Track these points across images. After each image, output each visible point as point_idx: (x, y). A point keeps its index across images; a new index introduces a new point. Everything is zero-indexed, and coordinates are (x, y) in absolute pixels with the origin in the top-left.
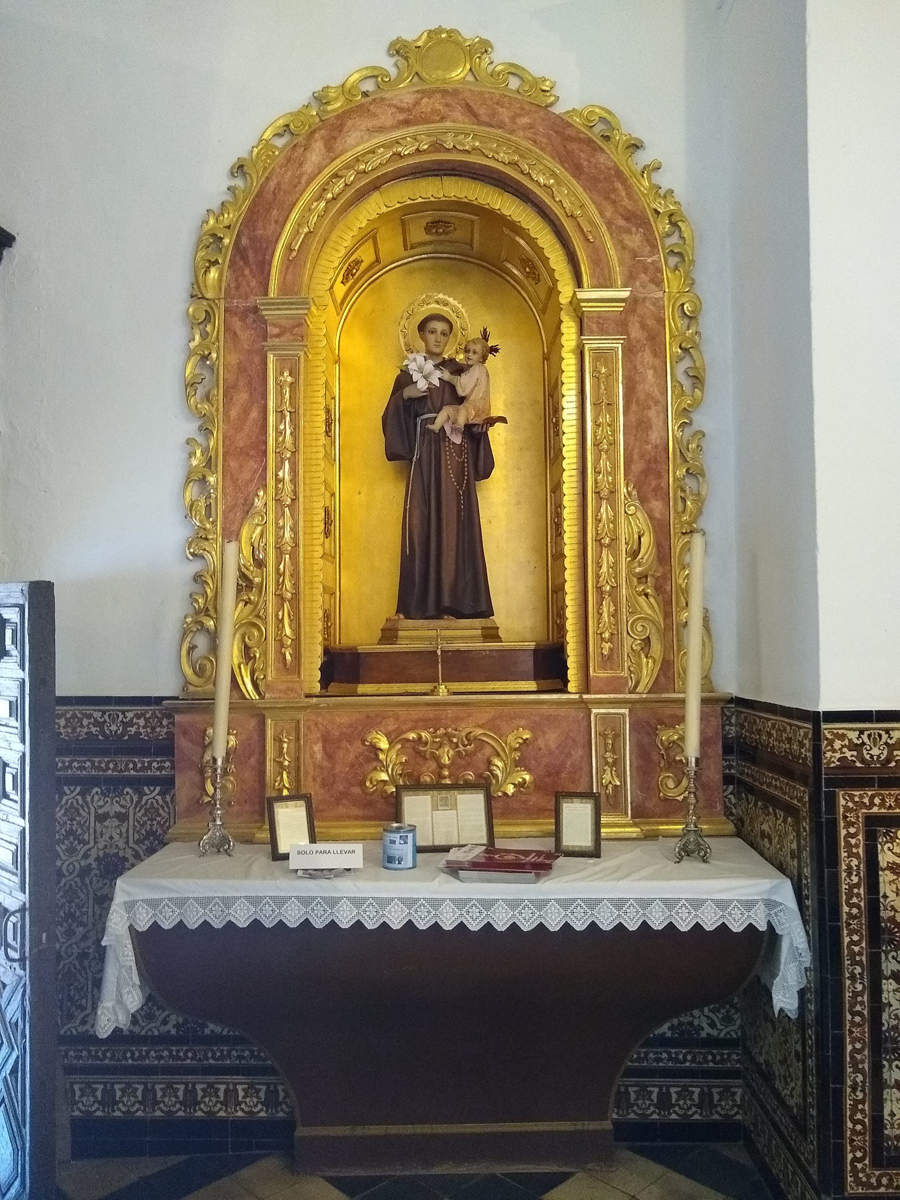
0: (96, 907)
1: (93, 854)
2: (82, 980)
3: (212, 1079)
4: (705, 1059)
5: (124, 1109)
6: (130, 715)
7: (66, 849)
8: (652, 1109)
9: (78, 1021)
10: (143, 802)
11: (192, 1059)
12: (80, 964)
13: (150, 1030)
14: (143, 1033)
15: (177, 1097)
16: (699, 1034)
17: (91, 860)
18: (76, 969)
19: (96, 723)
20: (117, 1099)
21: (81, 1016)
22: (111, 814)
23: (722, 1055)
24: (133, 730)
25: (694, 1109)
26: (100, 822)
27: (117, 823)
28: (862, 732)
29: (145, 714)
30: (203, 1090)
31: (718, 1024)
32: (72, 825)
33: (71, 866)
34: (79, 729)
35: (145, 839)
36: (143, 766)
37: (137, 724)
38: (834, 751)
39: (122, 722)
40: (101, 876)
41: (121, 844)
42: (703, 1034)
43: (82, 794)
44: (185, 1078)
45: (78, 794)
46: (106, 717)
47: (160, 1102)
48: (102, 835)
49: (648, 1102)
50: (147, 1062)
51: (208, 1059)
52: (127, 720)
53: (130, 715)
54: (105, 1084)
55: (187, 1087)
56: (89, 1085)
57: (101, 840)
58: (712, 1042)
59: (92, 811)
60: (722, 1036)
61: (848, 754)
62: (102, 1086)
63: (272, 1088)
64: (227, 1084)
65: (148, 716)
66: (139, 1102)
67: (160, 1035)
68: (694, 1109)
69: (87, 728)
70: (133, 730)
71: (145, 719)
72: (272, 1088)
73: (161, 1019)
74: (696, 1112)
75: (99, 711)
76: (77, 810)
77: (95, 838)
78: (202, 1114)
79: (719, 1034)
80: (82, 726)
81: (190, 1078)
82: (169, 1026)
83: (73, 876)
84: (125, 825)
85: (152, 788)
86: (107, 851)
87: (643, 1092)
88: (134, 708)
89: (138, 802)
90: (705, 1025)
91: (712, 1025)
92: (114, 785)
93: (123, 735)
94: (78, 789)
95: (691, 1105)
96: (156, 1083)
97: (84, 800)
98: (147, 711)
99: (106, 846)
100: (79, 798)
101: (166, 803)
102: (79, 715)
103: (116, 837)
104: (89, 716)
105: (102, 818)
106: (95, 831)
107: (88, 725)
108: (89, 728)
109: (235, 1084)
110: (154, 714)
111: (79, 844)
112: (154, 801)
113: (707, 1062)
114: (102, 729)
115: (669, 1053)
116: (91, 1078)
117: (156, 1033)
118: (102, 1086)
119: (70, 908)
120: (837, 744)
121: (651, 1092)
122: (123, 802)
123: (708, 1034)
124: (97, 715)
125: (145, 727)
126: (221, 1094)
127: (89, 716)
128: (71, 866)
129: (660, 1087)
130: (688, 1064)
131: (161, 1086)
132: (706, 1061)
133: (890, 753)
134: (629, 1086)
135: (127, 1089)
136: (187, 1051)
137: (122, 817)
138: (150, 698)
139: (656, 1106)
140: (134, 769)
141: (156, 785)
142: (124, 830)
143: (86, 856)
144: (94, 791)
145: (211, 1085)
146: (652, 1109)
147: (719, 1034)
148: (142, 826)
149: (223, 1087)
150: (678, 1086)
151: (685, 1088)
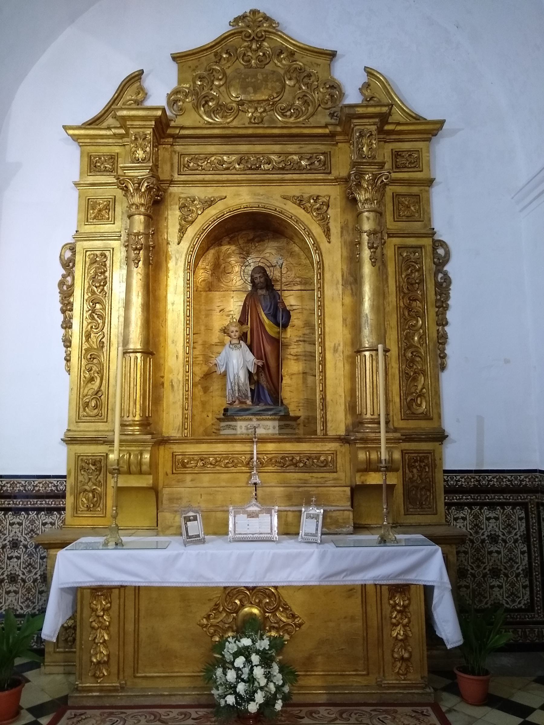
1: (8, 539)
2: (518, 586)
6: (458, 477)
9: (517, 602)
15: (518, 634)
19: (54, 486)
24: (524, 483)
27: (462, 521)
28: (448, 476)
31: (24, 608)
38: (471, 482)
42: (18, 613)
43: (512, 509)
46: (59, 483)
51: (526, 618)
59: (41, 521)
60: (478, 608)
65: (530, 477)
69: (505, 483)
70: (524, 483)
73: (485, 602)
76: (511, 516)
77: (9, 532)
82: (522, 605)
84: (466, 522)
89: (503, 512)
90: (19, 609)
91: (507, 603)
92: (492, 506)
93: (33, 490)
94: (35, 512)
97: (37, 517)
98: (529, 475)
101: (482, 513)
102: (16, 483)
104: (506, 478)
105: (12, 524)
117: (516, 607)
120: (18, 485)
121: (518, 631)
124: (509, 477)
125: (10, 487)
130: (518, 620)
133: (521, 483)
137: (496, 519)
138: (18, 476)
140: (30, 504)
141: (34, 511)
142: (498, 524)
143: (5, 540)
149: (537, 630)
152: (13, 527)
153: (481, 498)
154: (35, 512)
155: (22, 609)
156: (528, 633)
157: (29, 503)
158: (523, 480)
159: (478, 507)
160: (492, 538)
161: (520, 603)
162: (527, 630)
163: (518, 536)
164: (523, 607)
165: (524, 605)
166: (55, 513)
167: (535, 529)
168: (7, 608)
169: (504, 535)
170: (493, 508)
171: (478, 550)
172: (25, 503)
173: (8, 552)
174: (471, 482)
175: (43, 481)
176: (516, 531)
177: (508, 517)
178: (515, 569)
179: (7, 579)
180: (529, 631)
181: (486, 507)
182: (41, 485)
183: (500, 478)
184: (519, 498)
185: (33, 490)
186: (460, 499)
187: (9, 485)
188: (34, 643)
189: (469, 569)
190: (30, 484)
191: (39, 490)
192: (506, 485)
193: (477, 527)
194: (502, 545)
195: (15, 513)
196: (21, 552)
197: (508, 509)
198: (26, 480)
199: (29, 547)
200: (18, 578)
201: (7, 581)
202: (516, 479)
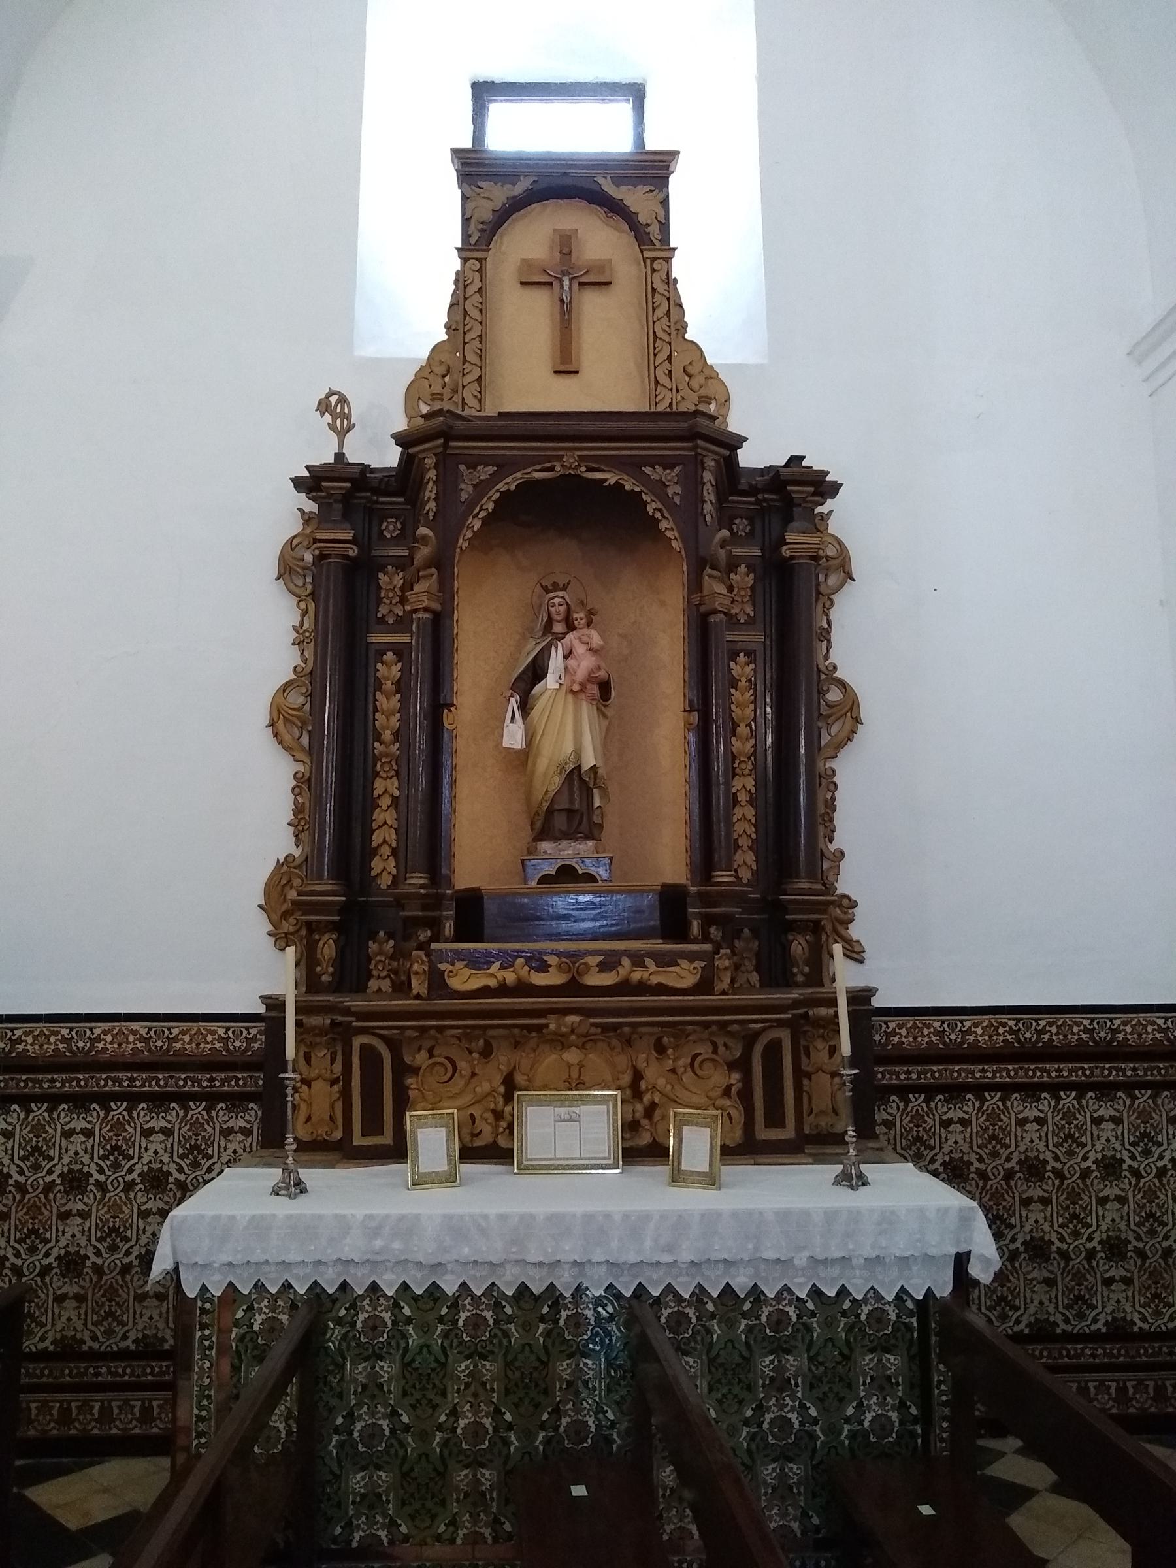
0: (1099, 1208)
3: (1142, 1375)
4: (1060, 1354)
5: (121, 1426)
6: (968, 1024)
7: (31, 1166)
8: (134, 1423)
10: (985, 1108)
11: (1125, 1356)
12: (42, 1281)
13: (1159, 1326)
14: (1152, 1330)
15: (1109, 1394)
16: (80, 1348)
17: (1013, 1163)
18: (118, 1284)
20: (33, 1417)
21: (122, 1332)
22: (78, 1130)
23: (1153, 1348)
24: (1047, 1037)
25: (93, 1424)
26: (66, 1138)
27: (162, 1138)
29: (1056, 1022)
30: (1095, 1387)
32: (1070, 1129)
33: (116, 1186)
34: (995, 1038)
35: (188, 1154)
36: (229, 1082)
37: (975, 1032)
38: (999, 1035)
39: (89, 1038)
40: (65, 1191)
41: (1118, 1146)
42: (85, 1348)
44: (1117, 1375)
45: (1149, 1098)
47: (75, 1420)
48: (146, 1149)
49: (89, 1417)
50: (1082, 1359)
52: (251, 1036)
53: (968, 1024)
54: (1117, 1381)
55: (143, 1403)
56: (126, 1402)
57: (145, 1155)
58: (1144, 1336)
61: (217, 1045)
62: (140, 1403)
63: (106, 1404)
64: (1079, 1382)
66: (96, 1420)
67: (1015, 1333)
68: (93, 1424)
71: (1057, 1026)
72: (1083, 1385)
74: (95, 1427)
75: (1088, 1018)
78: (1135, 1411)
79: (1150, 1327)
80: (923, 1036)
81: (147, 1394)
83: (37, 1193)
85: (39, 1105)
86: (72, 1167)
87: (85, 1407)
88: (21, 1026)
89: (980, 1108)
92: (1105, 1090)
95: (91, 1420)
96: (112, 1400)
97: (130, 1115)
99: (150, 1162)
100: (125, 1113)
103: (961, 1142)
104: (1004, 1025)
106: (1016, 1135)
107: (55, 1042)
108: (56, 1045)
109: (1086, 1382)
110: (1065, 1022)
111: (925, 1149)
112: (121, 1117)
113: (146, 1375)
114: (226, 1045)
115: (109, 1368)
116: (129, 1395)
117: (115, 1349)
118: (140, 1403)
119: (114, 1223)
122: (247, 1117)
123: (90, 1347)
126: (96, 1411)
127: (56, 1033)
128: (116, 1186)
129: (102, 1402)
130: (127, 1378)
131: (118, 1403)
132: (63, 1375)
133: (13, 1046)
134: (112, 1400)
135: (1140, 1385)
136: (44, 1368)
139: (56, 1422)
141: (43, 1102)
144: (141, 1106)
145: (1102, 1383)
146: (134, 1423)
147: (1150, 1327)
148: (27, 1143)
150: (119, 1400)
151: (85, 1403)
152: (151, 1139)
153: (177, 1083)
154: (999, 1094)
155: (1144, 1320)
156: (34, 1412)
157: (162, 1083)
158: (1043, 1031)
159: (1149, 1092)
160: (1030, 1167)
161: (125, 1337)
162: (114, 1404)
163: (1089, 1163)
164: (133, 1347)
165: (135, 1341)
166: (15, 1106)
167: (106, 1084)
168: (58, 1336)
169: (981, 1160)
170: (1033, 1096)
171: (1074, 1196)
172: (1021, 1073)
173: (60, 1200)
174: (999, 1035)
175: (114, 1027)
176: (1162, 1148)
177: (197, 1127)
178: (40, 1257)
179: (1026, 1251)
180: (119, 1407)
181: (1166, 1093)
182: (109, 1038)
183: (121, 1032)
184: (937, 1075)
185: (10, 1052)
186: (70, 1080)
187: (187, 1038)
188: (1149, 1402)
189: (1131, 1238)
190: (952, 1027)
191: (105, 1050)
192: (930, 1043)
193: (36, 1154)
194: (1130, 1183)
195: (234, 1105)
196: (10, 1203)
197: (119, 1109)
198: (227, 1024)
199: (30, 1190)
200: (84, 1263)
201: (137, 1269)
202: (952, 1027)
